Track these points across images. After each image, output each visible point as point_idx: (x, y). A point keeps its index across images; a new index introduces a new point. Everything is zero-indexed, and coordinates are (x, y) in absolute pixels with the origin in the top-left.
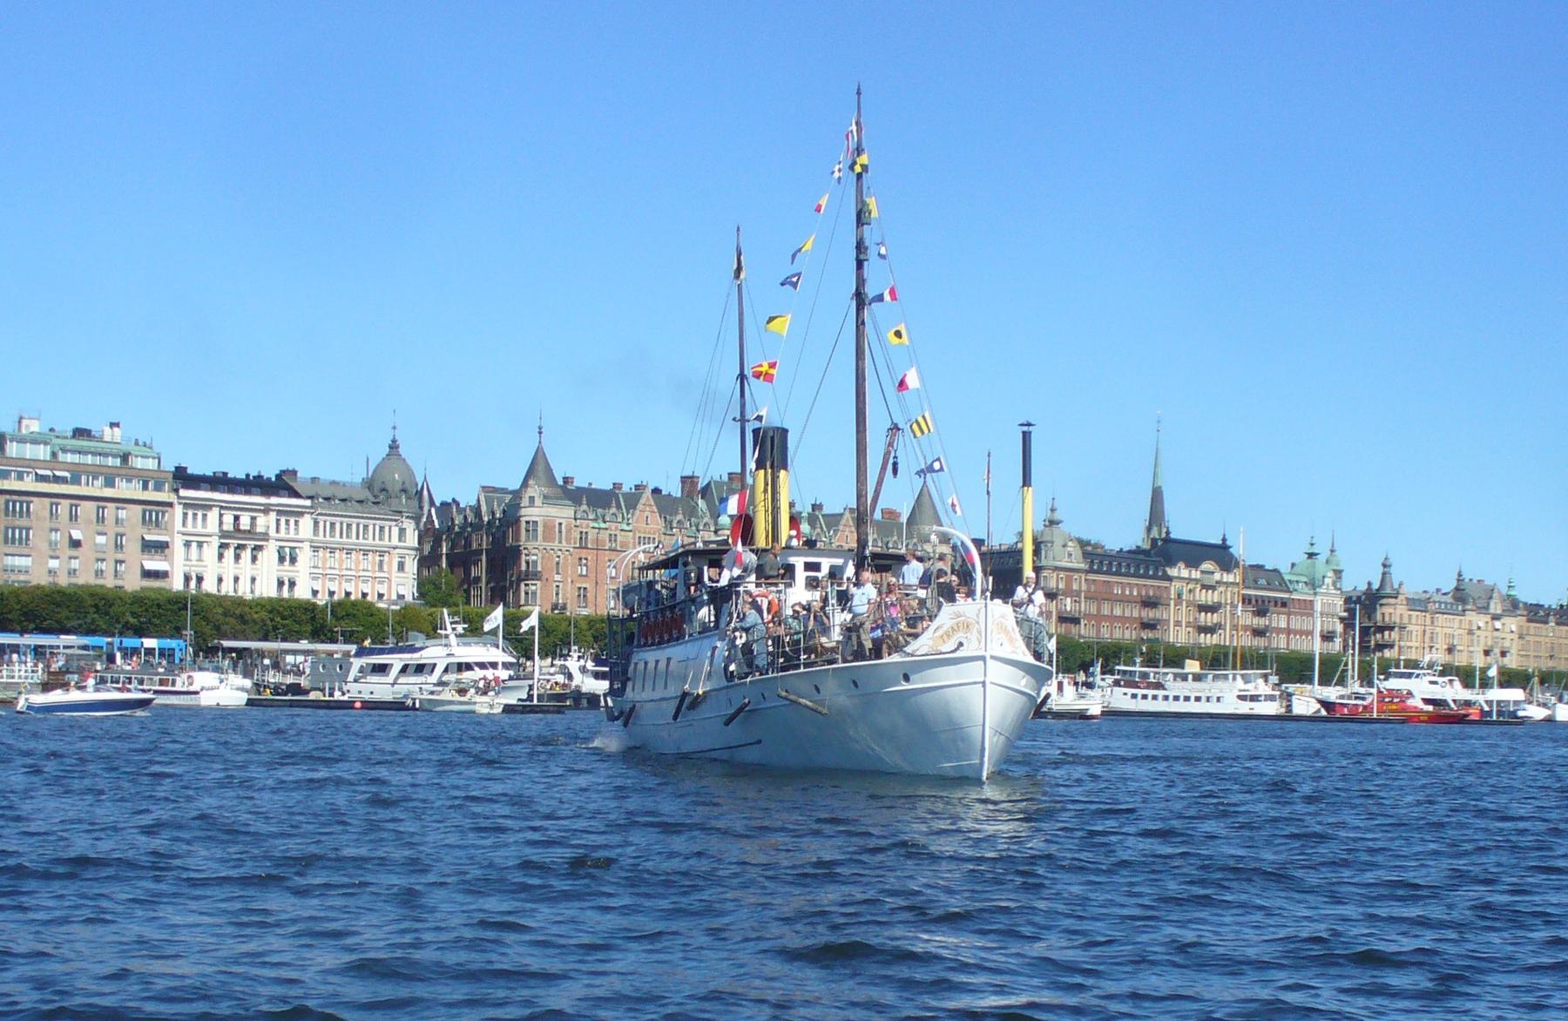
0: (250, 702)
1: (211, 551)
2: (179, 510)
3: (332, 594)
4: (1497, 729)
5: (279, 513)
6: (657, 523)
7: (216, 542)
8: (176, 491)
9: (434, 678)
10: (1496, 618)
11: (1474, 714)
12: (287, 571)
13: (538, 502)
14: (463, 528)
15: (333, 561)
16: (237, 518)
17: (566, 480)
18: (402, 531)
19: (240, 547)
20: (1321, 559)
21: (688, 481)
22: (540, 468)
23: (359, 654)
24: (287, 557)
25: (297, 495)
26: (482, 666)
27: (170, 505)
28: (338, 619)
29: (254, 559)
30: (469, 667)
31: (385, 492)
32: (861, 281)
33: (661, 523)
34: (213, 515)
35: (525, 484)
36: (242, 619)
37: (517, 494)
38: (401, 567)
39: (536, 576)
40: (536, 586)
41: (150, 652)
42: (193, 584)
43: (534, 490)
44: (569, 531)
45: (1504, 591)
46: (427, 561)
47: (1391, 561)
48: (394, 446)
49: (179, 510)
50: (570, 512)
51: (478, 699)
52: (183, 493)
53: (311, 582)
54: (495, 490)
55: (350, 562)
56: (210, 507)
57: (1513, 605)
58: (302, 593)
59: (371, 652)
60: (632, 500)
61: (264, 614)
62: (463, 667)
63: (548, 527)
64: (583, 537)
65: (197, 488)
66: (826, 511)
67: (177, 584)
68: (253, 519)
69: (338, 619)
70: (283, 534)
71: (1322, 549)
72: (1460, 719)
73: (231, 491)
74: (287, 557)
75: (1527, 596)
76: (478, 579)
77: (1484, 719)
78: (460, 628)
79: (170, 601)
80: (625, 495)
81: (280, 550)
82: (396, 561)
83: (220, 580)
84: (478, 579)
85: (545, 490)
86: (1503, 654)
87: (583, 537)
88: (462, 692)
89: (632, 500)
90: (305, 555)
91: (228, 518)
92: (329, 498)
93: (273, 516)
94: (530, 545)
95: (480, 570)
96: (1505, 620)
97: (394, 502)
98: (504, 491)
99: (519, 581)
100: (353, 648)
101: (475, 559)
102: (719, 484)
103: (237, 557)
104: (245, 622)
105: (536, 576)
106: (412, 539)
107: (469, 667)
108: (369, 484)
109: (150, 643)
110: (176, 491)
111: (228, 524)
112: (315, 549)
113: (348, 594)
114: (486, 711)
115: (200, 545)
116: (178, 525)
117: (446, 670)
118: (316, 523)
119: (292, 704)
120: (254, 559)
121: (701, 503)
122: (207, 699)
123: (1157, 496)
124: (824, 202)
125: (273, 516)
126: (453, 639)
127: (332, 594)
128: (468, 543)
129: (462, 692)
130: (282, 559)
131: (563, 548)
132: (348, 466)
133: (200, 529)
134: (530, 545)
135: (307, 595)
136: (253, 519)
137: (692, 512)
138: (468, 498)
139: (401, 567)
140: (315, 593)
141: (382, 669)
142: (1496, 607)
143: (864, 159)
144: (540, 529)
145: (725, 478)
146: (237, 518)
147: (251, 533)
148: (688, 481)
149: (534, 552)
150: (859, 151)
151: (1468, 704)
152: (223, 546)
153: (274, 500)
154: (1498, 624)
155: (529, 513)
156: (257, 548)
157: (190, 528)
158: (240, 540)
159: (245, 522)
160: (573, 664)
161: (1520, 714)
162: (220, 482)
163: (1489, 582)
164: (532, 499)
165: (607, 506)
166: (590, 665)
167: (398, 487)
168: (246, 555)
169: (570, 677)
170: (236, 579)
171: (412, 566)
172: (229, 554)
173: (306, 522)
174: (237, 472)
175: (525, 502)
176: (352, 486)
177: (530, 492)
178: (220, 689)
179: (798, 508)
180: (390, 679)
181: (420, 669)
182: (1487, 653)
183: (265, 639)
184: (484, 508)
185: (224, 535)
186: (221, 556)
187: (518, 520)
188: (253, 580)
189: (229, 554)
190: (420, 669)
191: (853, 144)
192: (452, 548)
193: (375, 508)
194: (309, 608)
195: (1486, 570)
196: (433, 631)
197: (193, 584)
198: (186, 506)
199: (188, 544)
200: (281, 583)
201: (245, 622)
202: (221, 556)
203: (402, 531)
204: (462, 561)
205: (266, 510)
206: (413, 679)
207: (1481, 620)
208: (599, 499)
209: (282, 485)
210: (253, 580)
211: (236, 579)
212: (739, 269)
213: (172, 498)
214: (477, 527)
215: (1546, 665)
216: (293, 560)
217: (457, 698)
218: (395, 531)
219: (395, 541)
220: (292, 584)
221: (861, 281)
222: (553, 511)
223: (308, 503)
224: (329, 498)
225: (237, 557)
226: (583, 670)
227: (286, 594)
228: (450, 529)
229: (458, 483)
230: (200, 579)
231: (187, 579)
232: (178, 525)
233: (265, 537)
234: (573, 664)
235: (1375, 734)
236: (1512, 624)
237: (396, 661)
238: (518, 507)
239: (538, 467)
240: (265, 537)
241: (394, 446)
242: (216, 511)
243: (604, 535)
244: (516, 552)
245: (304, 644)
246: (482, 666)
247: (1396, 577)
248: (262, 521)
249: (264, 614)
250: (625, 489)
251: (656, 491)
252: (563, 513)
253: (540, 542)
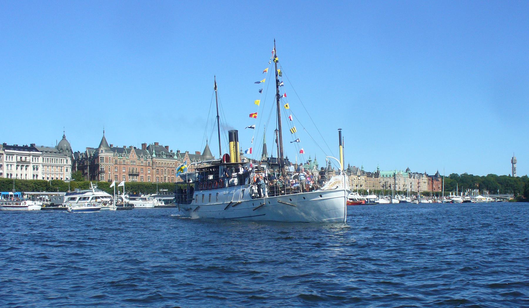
0: (42, 209)
1: (14, 167)
2: (5, 156)
3: (52, 178)
4: (369, 206)
5: (33, 156)
6: (136, 157)
7: (15, 164)
8: (4, 150)
9: (89, 201)
10: (359, 176)
11: (363, 202)
12: (35, 172)
13: (104, 152)
14: (82, 159)
15: (48, 169)
16: (21, 158)
17: (111, 145)
18: (67, 160)
19: (22, 166)
20: (312, 162)
21: (144, 145)
22: (104, 142)
23: (66, 195)
24: (35, 168)
25: (38, 151)
26: (102, 197)
27: (2, 154)
28: (53, 185)
29: (26, 169)
30: (99, 198)
31: (62, 150)
32: (278, 91)
33: (137, 156)
34: (15, 157)
35: (100, 147)
36: (27, 186)
37: (97, 150)
38: (67, 170)
39: (104, 172)
40: (103, 175)
41: (11, 196)
42: (9, 176)
43: (102, 148)
44: (112, 159)
45: (361, 169)
46: (73, 168)
47: (516, 158)
48: (64, 137)
49: (5, 156)
50: (112, 154)
51: (110, 206)
52: (6, 151)
53: (42, 175)
54: (90, 148)
55: (53, 169)
56: (14, 155)
57: (363, 173)
58: (40, 178)
59: (71, 194)
60: (129, 151)
61: (33, 184)
62: (97, 198)
63: (107, 159)
64: (116, 161)
65: (10, 149)
66: (181, 152)
67: (5, 176)
68: (26, 158)
69: (53, 185)
70: (34, 162)
71: (313, 159)
72: (360, 204)
73: (19, 150)
74: (35, 168)
75: (367, 170)
76: (87, 173)
77: (366, 203)
78: (95, 187)
79: (6, 181)
80: (127, 149)
81: (33, 166)
82: (65, 169)
83: (17, 175)
84: (87, 173)
85: (106, 148)
86: (361, 186)
87: (116, 161)
88: (105, 204)
89: (129, 151)
90: (40, 168)
91: (19, 158)
92: (46, 152)
93: (31, 157)
94: (102, 163)
95: (87, 171)
96: (361, 177)
97: (65, 152)
98: (93, 149)
99: (99, 173)
100: (65, 193)
101: (87, 168)
102: (152, 146)
103: (22, 169)
104: (28, 187)
105: (104, 172)
106: (70, 162)
107: (99, 198)
108: (57, 148)
109: (11, 193)
110: (4, 150)
111: (19, 159)
112: (43, 166)
113: (57, 178)
114: (112, 209)
115: (11, 165)
116: (5, 160)
117: (92, 199)
118: (43, 159)
119: (54, 209)
120: (26, 169)
121: (148, 151)
122: (30, 208)
123: (265, 146)
124: (267, 70)
125: (31, 157)
126: (94, 190)
127: (52, 178)
128: (84, 163)
129: (105, 204)
130: (34, 169)
131: (111, 164)
132: (52, 143)
133: (11, 161)
134: (102, 163)
135: (41, 179)
136: (26, 158)
137: (145, 154)
138: (83, 150)
139: (67, 170)
140: (43, 178)
141: (73, 199)
142: (359, 173)
143: (277, 59)
144: (104, 159)
145: (154, 144)
146: (21, 158)
147: (25, 162)
148: (144, 145)
149: (103, 165)
150: (276, 57)
151: (361, 200)
152: (18, 166)
153: (32, 152)
154: (359, 178)
155: (101, 155)
156: (27, 166)
157: (8, 161)
158: (22, 164)
159: (23, 159)
160: (123, 196)
161: (376, 202)
162: (16, 147)
163: (356, 167)
164: (102, 151)
165: (122, 152)
166: (128, 196)
167: (66, 148)
168: (24, 168)
169: (122, 200)
170: (21, 175)
171: (70, 170)
172: (19, 168)
173: (41, 158)
174: (20, 145)
175: (100, 152)
176: (52, 148)
177: (102, 149)
178: (34, 206)
179: (173, 152)
180: (76, 202)
181: (85, 199)
182: (357, 186)
183: (33, 191)
184: (88, 154)
185: (18, 162)
186: (17, 168)
187: (98, 157)
188: (26, 175)
189: (19, 168)
190: (85, 199)
191: (274, 55)
192: (79, 165)
193: (59, 154)
194: (46, 182)
195: (356, 164)
196: (86, 187)
197: (9, 176)
198: (7, 154)
199: (8, 165)
200: (34, 176)
201: (28, 187)
202: (17, 168)
203: (67, 160)
204: (82, 168)
205: (29, 155)
206: (83, 202)
207: (355, 177)
208: (120, 151)
209: (32, 148)
210: (26, 175)
211: (21, 175)
212: (216, 87)
213: (3, 152)
214: (86, 159)
215: (372, 189)
216: (37, 169)
217: (104, 206)
218: (65, 160)
219: (65, 163)
220: (37, 176)
221: (278, 91)
222: (108, 154)
223: (41, 153)
224: (46, 152)
225: (22, 169)
226: (126, 198)
227: (35, 178)
228: (78, 160)
229: (80, 146)
230: (11, 175)
231: (8, 175)
232: (5, 160)
233: (29, 163)
234: (123, 196)
235: (369, 208)
236: (363, 178)
237: (78, 197)
238: (98, 153)
239: (103, 142)
240: (29, 163)
241: (64, 137)
242: (15, 156)
243: (122, 160)
244: (98, 166)
245: (44, 193)
246: (102, 197)
247: (332, 166)
248: (28, 158)
249: (33, 184)
250: (127, 148)
251: (135, 148)
252: (111, 155)
253: (105, 163)
